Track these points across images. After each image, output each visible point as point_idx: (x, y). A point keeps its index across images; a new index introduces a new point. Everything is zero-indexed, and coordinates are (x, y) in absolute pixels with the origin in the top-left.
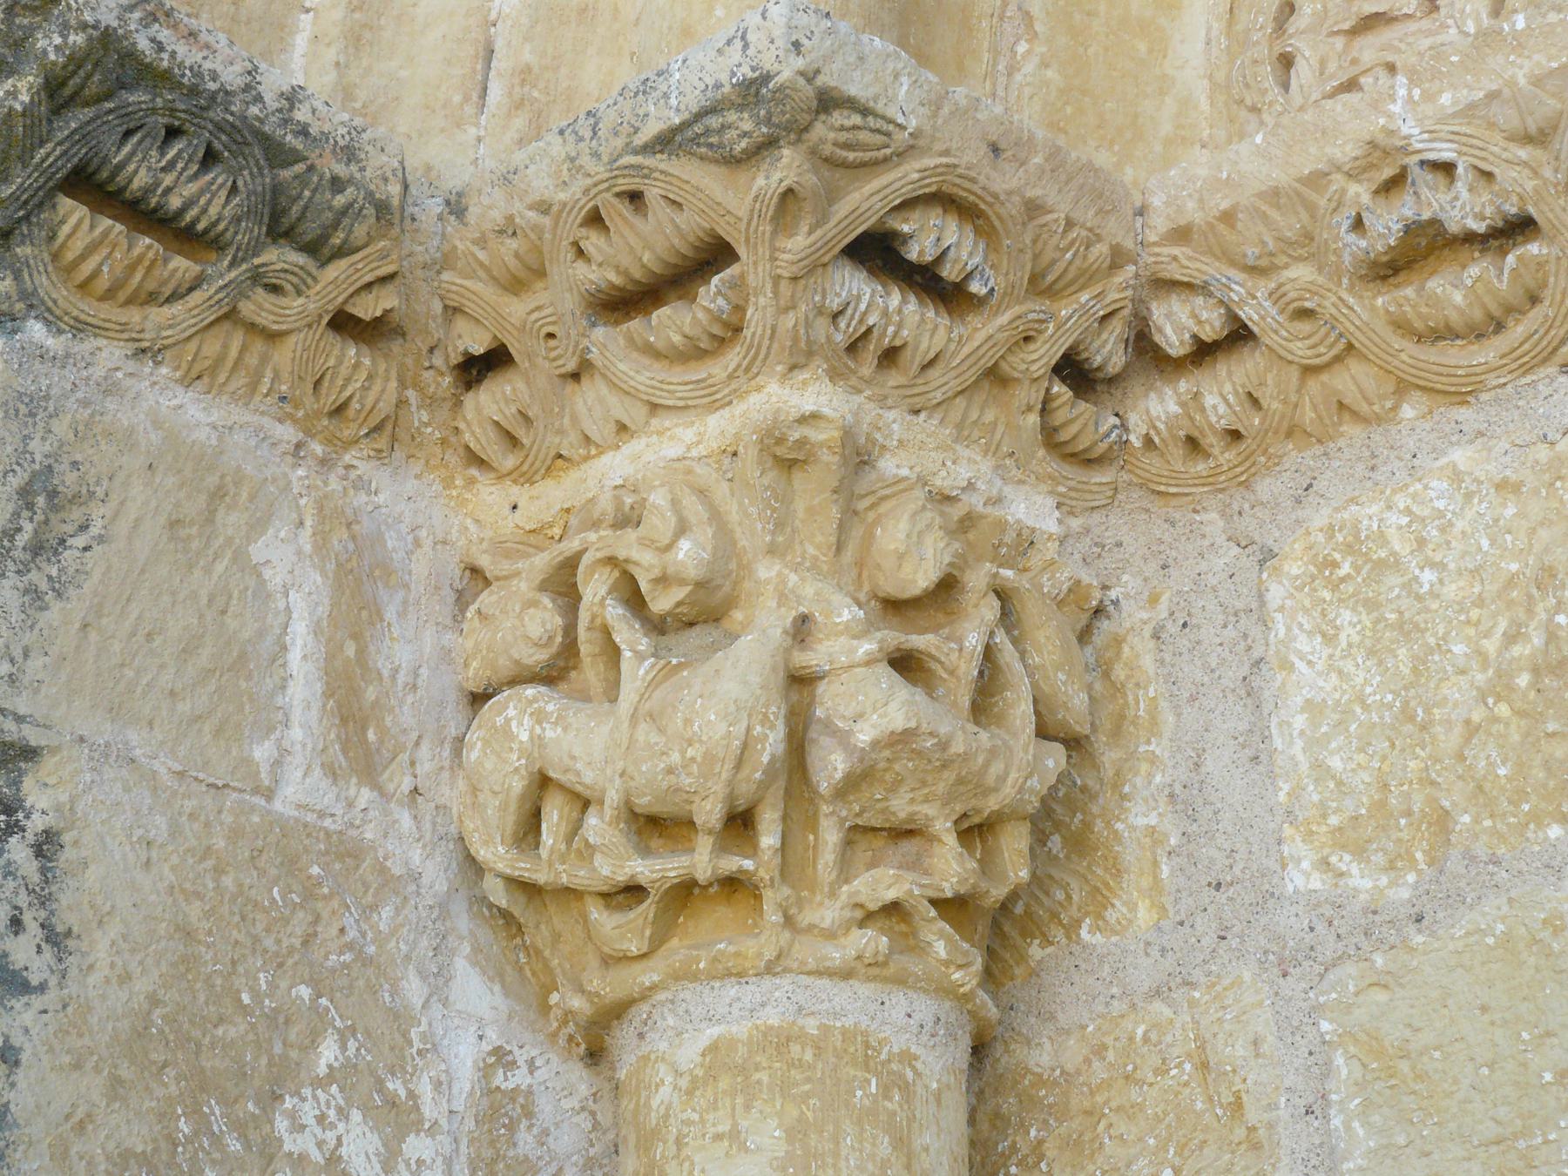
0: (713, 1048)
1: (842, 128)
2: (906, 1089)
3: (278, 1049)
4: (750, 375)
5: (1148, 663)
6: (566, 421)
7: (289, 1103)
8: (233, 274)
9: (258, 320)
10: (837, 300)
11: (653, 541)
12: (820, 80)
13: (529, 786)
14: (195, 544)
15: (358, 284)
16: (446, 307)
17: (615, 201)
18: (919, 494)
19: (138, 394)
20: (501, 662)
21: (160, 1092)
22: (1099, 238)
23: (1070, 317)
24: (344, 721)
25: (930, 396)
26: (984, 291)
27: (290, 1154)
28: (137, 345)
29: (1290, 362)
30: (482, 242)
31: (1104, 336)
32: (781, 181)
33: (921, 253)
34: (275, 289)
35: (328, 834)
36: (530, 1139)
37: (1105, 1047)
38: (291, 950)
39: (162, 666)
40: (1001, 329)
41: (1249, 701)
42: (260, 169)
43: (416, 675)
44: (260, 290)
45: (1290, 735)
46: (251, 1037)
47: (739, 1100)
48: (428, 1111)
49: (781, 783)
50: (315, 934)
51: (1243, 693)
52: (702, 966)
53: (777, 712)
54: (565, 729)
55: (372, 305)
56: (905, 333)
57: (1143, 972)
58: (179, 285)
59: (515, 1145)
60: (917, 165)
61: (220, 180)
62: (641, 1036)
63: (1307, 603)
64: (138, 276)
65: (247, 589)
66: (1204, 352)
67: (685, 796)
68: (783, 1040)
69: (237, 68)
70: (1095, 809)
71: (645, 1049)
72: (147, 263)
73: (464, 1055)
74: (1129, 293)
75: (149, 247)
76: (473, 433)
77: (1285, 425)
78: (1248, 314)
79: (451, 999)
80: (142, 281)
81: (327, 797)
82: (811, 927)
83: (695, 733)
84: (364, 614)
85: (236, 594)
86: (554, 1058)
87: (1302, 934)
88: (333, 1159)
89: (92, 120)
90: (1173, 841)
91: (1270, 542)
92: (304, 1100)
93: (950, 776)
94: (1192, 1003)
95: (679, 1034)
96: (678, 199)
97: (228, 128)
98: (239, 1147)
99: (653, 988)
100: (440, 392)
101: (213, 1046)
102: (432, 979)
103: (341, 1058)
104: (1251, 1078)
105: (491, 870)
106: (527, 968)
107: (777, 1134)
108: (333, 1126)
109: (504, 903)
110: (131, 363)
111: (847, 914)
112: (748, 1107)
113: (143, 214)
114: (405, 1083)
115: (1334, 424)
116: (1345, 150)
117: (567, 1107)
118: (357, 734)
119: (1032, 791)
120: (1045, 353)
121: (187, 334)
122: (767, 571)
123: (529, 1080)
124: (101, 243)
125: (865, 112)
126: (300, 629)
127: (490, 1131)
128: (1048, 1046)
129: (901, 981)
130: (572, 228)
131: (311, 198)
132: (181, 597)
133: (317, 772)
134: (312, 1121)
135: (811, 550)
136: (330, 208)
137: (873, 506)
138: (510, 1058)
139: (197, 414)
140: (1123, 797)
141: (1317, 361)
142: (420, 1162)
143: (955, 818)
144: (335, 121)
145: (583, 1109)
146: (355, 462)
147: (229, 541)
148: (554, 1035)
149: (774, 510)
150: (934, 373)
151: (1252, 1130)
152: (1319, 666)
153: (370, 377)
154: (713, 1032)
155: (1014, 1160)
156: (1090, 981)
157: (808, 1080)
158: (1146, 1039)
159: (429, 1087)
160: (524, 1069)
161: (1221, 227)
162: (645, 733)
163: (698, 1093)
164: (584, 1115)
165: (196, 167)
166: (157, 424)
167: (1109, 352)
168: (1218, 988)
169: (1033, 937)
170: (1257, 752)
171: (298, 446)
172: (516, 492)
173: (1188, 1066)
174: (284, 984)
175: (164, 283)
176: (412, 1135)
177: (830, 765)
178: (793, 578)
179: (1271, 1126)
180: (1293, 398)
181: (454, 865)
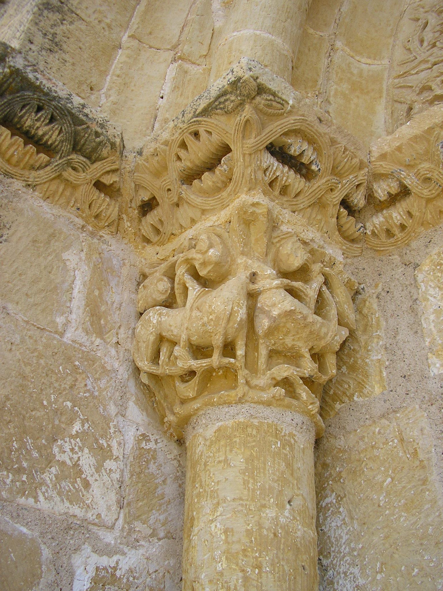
0: (219, 430)
1: (267, 100)
2: (291, 447)
3: (57, 422)
4: (235, 193)
5: (375, 306)
6: (174, 220)
7: (59, 442)
8: (61, 161)
9: (69, 179)
10: (265, 164)
11: (201, 250)
12: (258, 81)
13: (156, 338)
14: (41, 249)
15: (104, 171)
16: (136, 185)
17: (189, 136)
18: (295, 239)
19: (26, 199)
20: (149, 300)
21: (7, 431)
22: (356, 157)
23: (346, 183)
24: (92, 315)
25: (299, 206)
26: (317, 169)
27: (59, 461)
28: (27, 183)
29: (422, 198)
30: (147, 160)
31: (358, 192)
32: (245, 116)
33: (295, 151)
34: (74, 169)
35: (83, 352)
36: (154, 467)
37: (364, 437)
38: (65, 389)
39: (24, 285)
40: (323, 184)
41: (413, 314)
42: (70, 124)
43: (121, 305)
44: (70, 169)
46: (46, 417)
47: (228, 448)
48: (115, 453)
49: (245, 330)
50: (75, 385)
51: (410, 312)
52: (215, 400)
53: (244, 303)
54: (168, 317)
55: (109, 179)
56: (290, 181)
58: (42, 163)
59: (148, 469)
60: (293, 118)
61: (56, 127)
62: (194, 428)
63: (432, 278)
64: (27, 158)
65: (60, 267)
66: (393, 199)
67: (209, 334)
68: (245, 427)
69: (65, 92)
70: (358, 356)
71: (195, 432)
72: (30, 153)
73: (130, 435)
74: (366, 177)
75: (31, 148)
76: (145, 230)
77: (421, 220)
78: (407, 182)
79: (127, 415)
80: (29, 160)
81: (83, 338)
82: (256, 386)
83: (213, 310)
84: (103, 283)
85: (55, 267)
86: (165, 441)
87: (438, 389)
88: (76, 465)
89: (12, 99)
90: (387, 363)
91: (417, 262)
92: (66, 442)
93: (307, 331)
94: (397, 419)
95: (207, 426)
96: (210, 130)
97: (59, 108)
98: (37, 455)
99: (198, 409)
100: (134, 216)
101: (30, 418)
102: (119, 407)
103: (82, 429)
104: (421, 442)
105: (143, 370)
106: (156, 408)
107: (242, 460)
108: (77, 453)
109: (147, 382)
110: (25, 189)
111: (270, 381)
112: (231, 451)
113: (29, 138)
114: (107, 441)
115: (438, 219)
117: (169, 457)
118: (96, 318)
119: (337, 341)
120: (337, 196)
121: (44, 181)
122: (241, 260)
123: (155, 447)
124: (14, 144)
125: (274, 94)
126: (78, 285)
127: (139, 462)
128: (343, 438)
129: (289, 407)
130: (176, 149)
131: (88, 137)
132: (34, 264)
133: (80, 330)
134: (69, 450)
135: (257, 254)
136: (94, 141)
137: (279, 241)
138: (148, 438)
139: (47, 210)
140: (368, 351)
141: (432, 196)
142: (110, 470)
143: (309, 348)
144: (98, 116)
145: (175, 459)
146: (103, 235)
147: (55, 251)
148: (165, 432)
149: (244, 239)
150: (298, 198)
151: (421, 461)
153: (108, 205)
154: (220, 424)
155: (331, 479)
156: (358, 414)
157: (254, 441)
158: (379, 433)
159: (116, 444)
160: (154, 443)
161: (397, 152)
162: (196, 313)
163: (213, 446)
164: (175, 461)
165: (48, 121)
166: (32, 210)
167: (359, 200)
168: (406, 412)
169: (337, 401)
170: (417, 329)
171: (83, 227)
172: (158, 248)
173: (396, 441)
174: (61, 400)
175: (36, 161)
176: (108, 460)
177: (263, 324)
178: (250, 262)
179: (429, 459)
180: (424, 210)
181: (131, 370)
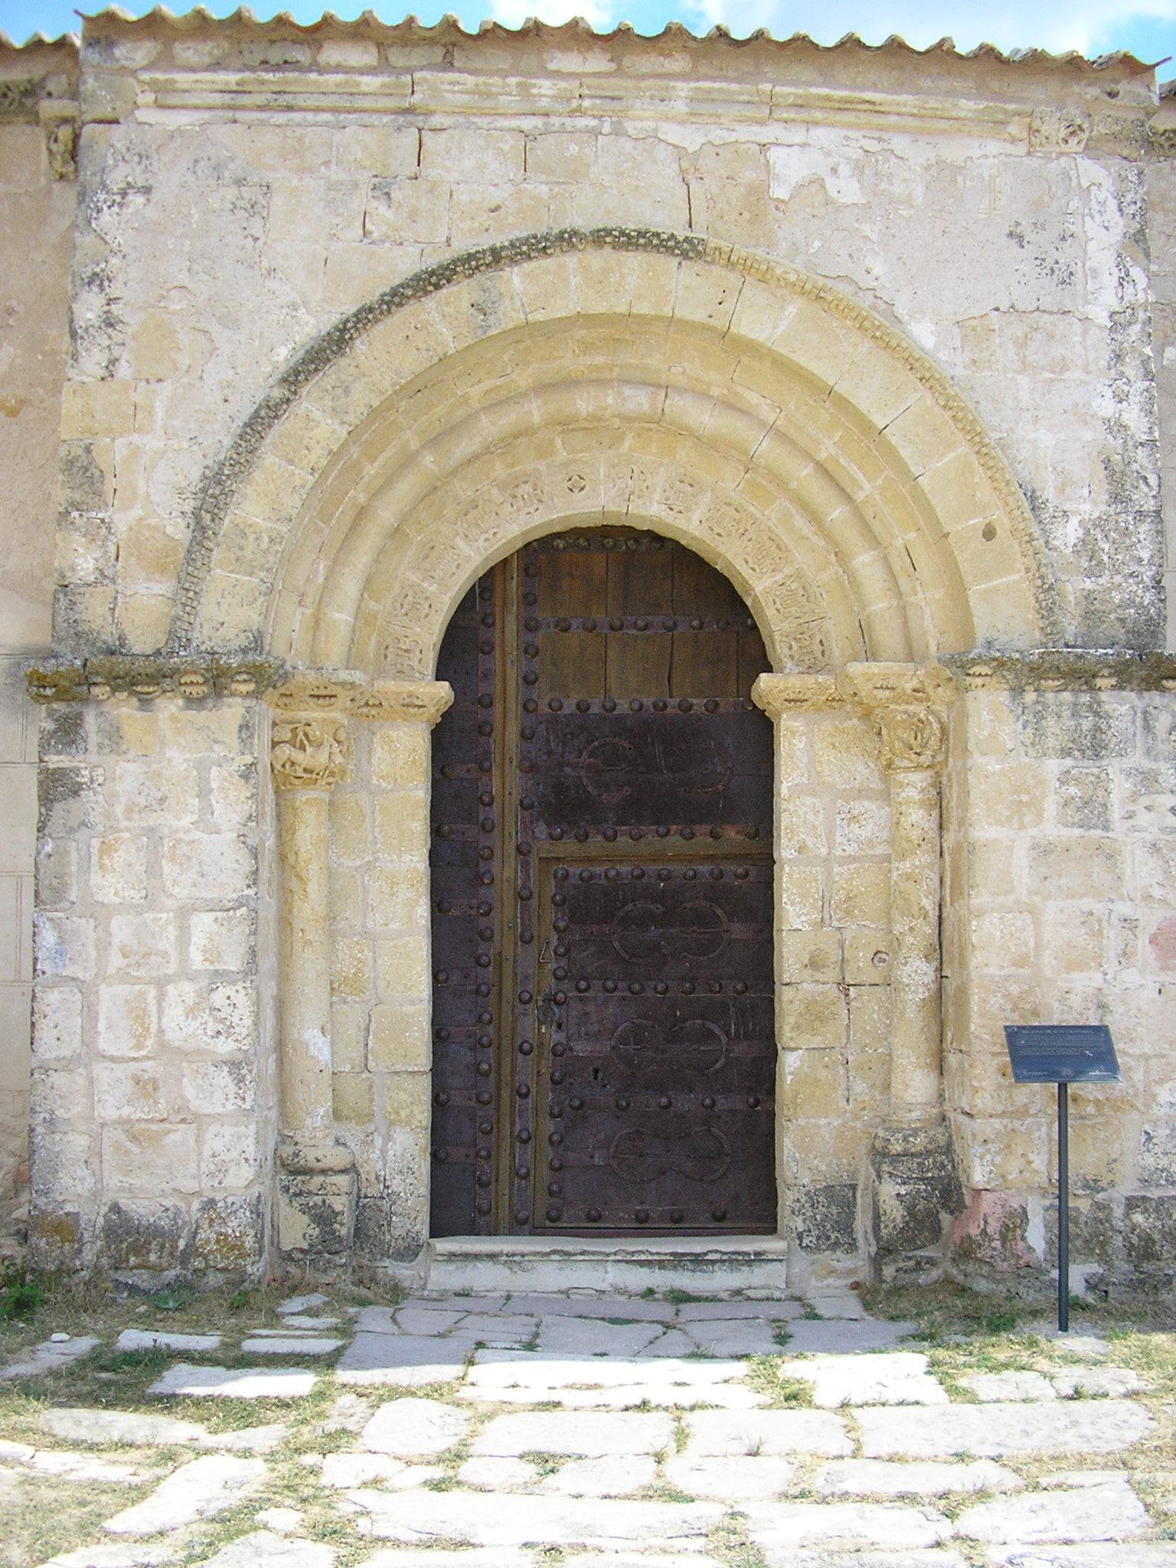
45: (375, 761)
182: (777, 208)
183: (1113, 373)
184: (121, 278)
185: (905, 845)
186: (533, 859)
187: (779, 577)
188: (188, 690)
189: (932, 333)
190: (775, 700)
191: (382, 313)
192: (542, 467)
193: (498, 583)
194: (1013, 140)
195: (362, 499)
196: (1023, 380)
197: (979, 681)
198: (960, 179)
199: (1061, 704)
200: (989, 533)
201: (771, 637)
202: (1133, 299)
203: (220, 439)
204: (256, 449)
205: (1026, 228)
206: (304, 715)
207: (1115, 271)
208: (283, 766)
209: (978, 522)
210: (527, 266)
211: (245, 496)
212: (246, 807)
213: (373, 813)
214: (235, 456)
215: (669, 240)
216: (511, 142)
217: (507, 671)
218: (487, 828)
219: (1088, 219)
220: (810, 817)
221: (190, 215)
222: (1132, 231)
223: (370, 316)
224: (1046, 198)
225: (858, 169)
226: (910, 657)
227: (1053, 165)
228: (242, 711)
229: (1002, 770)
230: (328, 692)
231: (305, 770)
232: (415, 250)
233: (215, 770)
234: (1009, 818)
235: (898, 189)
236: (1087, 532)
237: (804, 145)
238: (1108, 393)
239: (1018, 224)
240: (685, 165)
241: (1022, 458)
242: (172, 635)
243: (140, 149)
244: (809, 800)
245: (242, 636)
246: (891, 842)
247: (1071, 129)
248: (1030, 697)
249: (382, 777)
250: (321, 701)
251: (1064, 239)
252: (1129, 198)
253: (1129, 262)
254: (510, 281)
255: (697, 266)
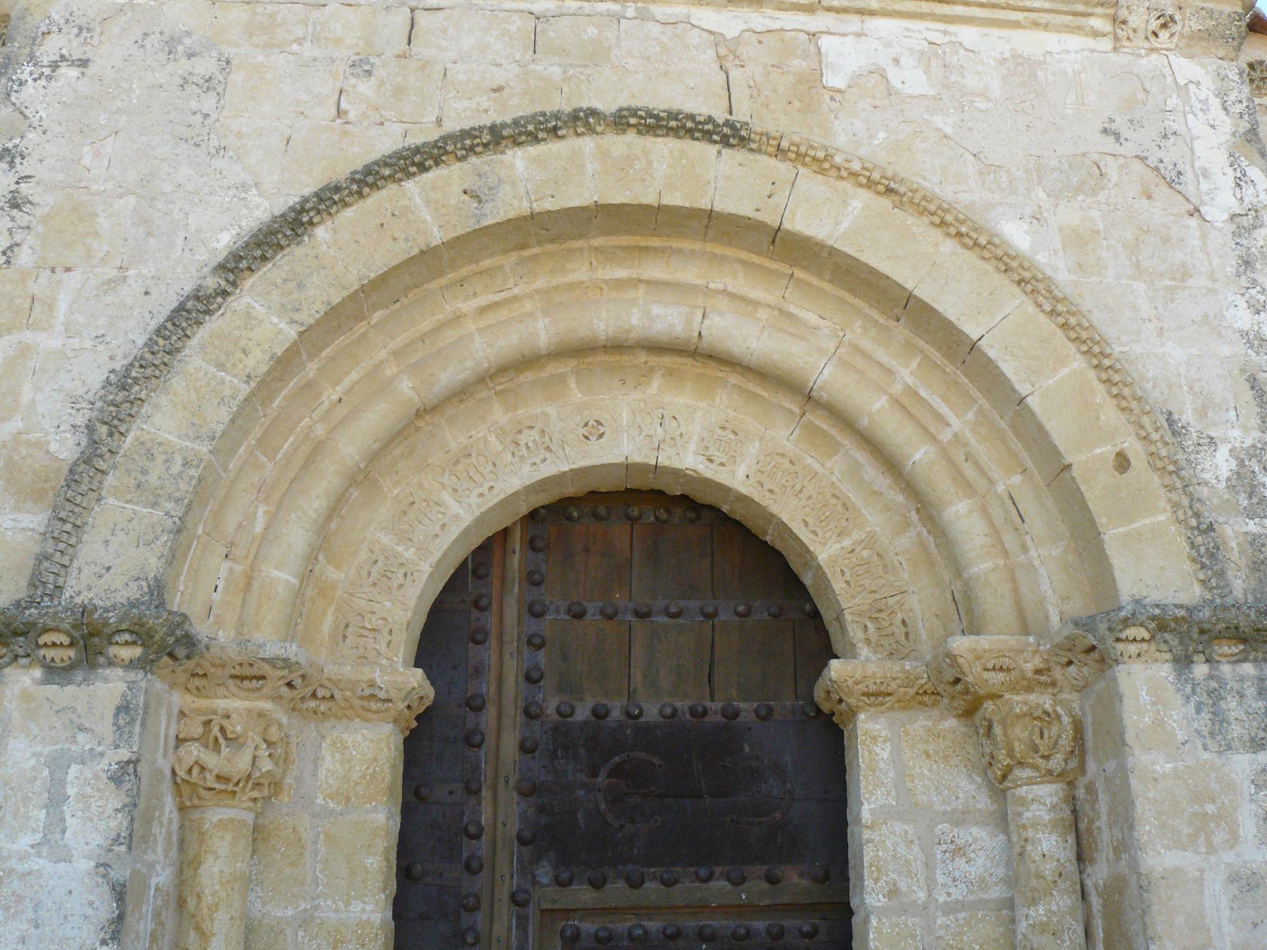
45: (322, 773)
57: (285, 810)
116: (365, 678)
152: (330, 762)
170: (314, 775)
182: (832, 99)
183: (1244, 281)
184: (36, 155)
185: (1034, 883)
186: (532, 911)
187: (847, 542)
188: (50, 653)
189: (1026, 232)
190: (851, 694)
191: (351, 194)
192: (551, 410)
193: (497, 555)
194: (1096, 34)
195: (320, 430)
196: (1140, 287)
197: (1133, 649)
198: (1040, 74)
199: (1242, 679)
200: (1122, 462)
201: (839, 618)
202: (1255, 200)
203: (131, 336)
204: (178, 350)
205: (1120, 124)
206: (222, 704)
207: (1230, 171)
208: (190, 771)
209: (1106, 450)
210: (532, 150)
211: (157, 407)
212: (113, 824)
213: (315, 843)
214: (148, 356)
215: (705, 123)
216: (519, 23)
217: (504, 667)
218: (473, 868)
219: (1190, 116)
220: (902, 849)
221: (133, 90)
222: (1242, 130)
223: (336, 197)
224: (1141, 95)
225: (924, 60)
226: (1025, 630)
227: (1143, 62)
228: (122, 687)
229: (1175, 769)
230: (254, 671)
231: (218, 777)
232: (398, 129)
233: (74, 770)
234: (1193, 838)
235: (971, 82)
236: (1241, 463)
237: (859, 35)
238: (1242, 303)
239: (1112, 120)
240: (723, 52)
241: (1150, 374)
242: (36, 580)
243: (82, 21)
244: (898, 827)
245: (133, 585)
246: (1011, 881)
247: (1162, 21)
248: (1200, 670)
249: (331, 796)
250: (246, 683)
251: (1165, 136)
252: (1233, 97)
253: (1244, 162)
254: (512, 166)
255: (740, 155)
